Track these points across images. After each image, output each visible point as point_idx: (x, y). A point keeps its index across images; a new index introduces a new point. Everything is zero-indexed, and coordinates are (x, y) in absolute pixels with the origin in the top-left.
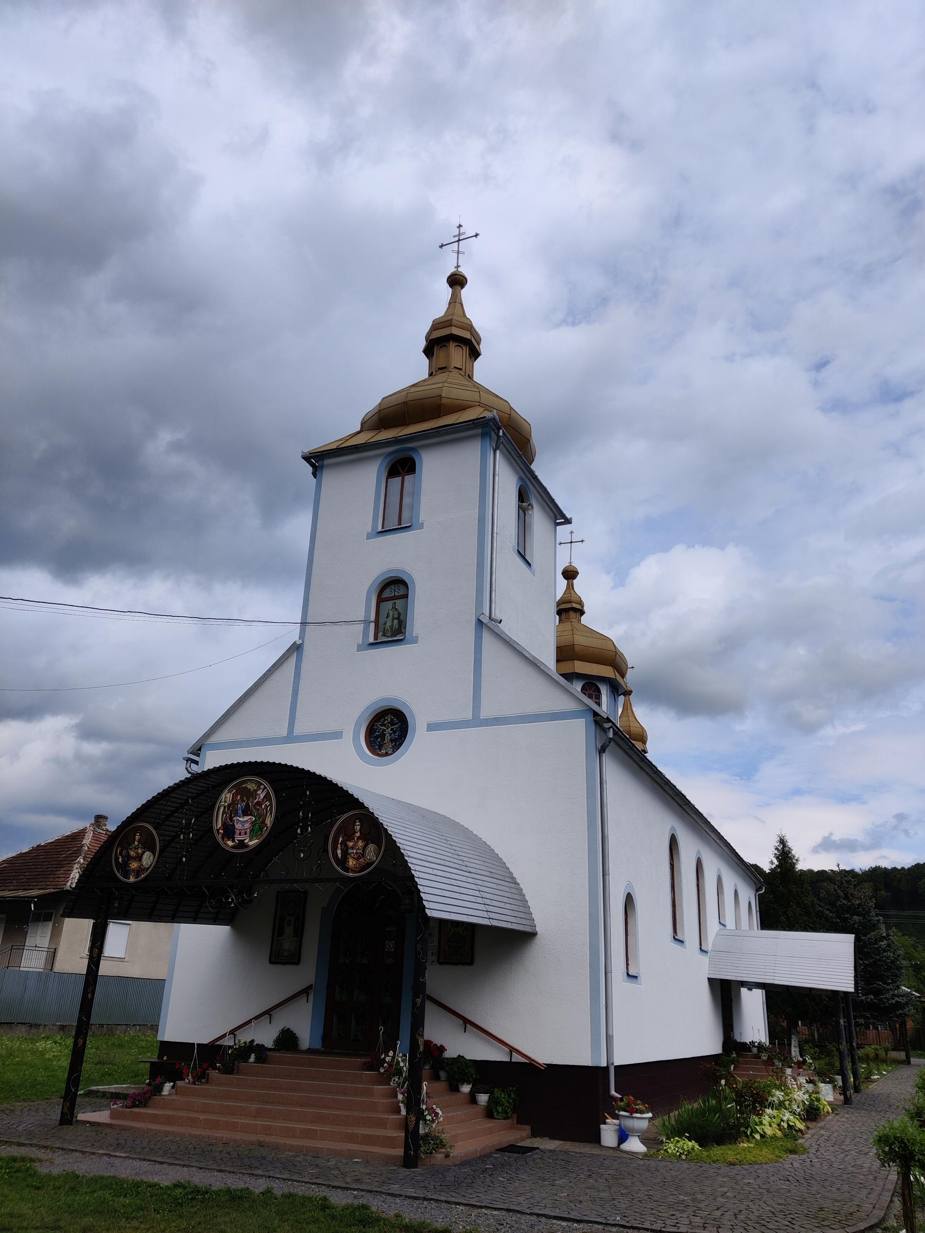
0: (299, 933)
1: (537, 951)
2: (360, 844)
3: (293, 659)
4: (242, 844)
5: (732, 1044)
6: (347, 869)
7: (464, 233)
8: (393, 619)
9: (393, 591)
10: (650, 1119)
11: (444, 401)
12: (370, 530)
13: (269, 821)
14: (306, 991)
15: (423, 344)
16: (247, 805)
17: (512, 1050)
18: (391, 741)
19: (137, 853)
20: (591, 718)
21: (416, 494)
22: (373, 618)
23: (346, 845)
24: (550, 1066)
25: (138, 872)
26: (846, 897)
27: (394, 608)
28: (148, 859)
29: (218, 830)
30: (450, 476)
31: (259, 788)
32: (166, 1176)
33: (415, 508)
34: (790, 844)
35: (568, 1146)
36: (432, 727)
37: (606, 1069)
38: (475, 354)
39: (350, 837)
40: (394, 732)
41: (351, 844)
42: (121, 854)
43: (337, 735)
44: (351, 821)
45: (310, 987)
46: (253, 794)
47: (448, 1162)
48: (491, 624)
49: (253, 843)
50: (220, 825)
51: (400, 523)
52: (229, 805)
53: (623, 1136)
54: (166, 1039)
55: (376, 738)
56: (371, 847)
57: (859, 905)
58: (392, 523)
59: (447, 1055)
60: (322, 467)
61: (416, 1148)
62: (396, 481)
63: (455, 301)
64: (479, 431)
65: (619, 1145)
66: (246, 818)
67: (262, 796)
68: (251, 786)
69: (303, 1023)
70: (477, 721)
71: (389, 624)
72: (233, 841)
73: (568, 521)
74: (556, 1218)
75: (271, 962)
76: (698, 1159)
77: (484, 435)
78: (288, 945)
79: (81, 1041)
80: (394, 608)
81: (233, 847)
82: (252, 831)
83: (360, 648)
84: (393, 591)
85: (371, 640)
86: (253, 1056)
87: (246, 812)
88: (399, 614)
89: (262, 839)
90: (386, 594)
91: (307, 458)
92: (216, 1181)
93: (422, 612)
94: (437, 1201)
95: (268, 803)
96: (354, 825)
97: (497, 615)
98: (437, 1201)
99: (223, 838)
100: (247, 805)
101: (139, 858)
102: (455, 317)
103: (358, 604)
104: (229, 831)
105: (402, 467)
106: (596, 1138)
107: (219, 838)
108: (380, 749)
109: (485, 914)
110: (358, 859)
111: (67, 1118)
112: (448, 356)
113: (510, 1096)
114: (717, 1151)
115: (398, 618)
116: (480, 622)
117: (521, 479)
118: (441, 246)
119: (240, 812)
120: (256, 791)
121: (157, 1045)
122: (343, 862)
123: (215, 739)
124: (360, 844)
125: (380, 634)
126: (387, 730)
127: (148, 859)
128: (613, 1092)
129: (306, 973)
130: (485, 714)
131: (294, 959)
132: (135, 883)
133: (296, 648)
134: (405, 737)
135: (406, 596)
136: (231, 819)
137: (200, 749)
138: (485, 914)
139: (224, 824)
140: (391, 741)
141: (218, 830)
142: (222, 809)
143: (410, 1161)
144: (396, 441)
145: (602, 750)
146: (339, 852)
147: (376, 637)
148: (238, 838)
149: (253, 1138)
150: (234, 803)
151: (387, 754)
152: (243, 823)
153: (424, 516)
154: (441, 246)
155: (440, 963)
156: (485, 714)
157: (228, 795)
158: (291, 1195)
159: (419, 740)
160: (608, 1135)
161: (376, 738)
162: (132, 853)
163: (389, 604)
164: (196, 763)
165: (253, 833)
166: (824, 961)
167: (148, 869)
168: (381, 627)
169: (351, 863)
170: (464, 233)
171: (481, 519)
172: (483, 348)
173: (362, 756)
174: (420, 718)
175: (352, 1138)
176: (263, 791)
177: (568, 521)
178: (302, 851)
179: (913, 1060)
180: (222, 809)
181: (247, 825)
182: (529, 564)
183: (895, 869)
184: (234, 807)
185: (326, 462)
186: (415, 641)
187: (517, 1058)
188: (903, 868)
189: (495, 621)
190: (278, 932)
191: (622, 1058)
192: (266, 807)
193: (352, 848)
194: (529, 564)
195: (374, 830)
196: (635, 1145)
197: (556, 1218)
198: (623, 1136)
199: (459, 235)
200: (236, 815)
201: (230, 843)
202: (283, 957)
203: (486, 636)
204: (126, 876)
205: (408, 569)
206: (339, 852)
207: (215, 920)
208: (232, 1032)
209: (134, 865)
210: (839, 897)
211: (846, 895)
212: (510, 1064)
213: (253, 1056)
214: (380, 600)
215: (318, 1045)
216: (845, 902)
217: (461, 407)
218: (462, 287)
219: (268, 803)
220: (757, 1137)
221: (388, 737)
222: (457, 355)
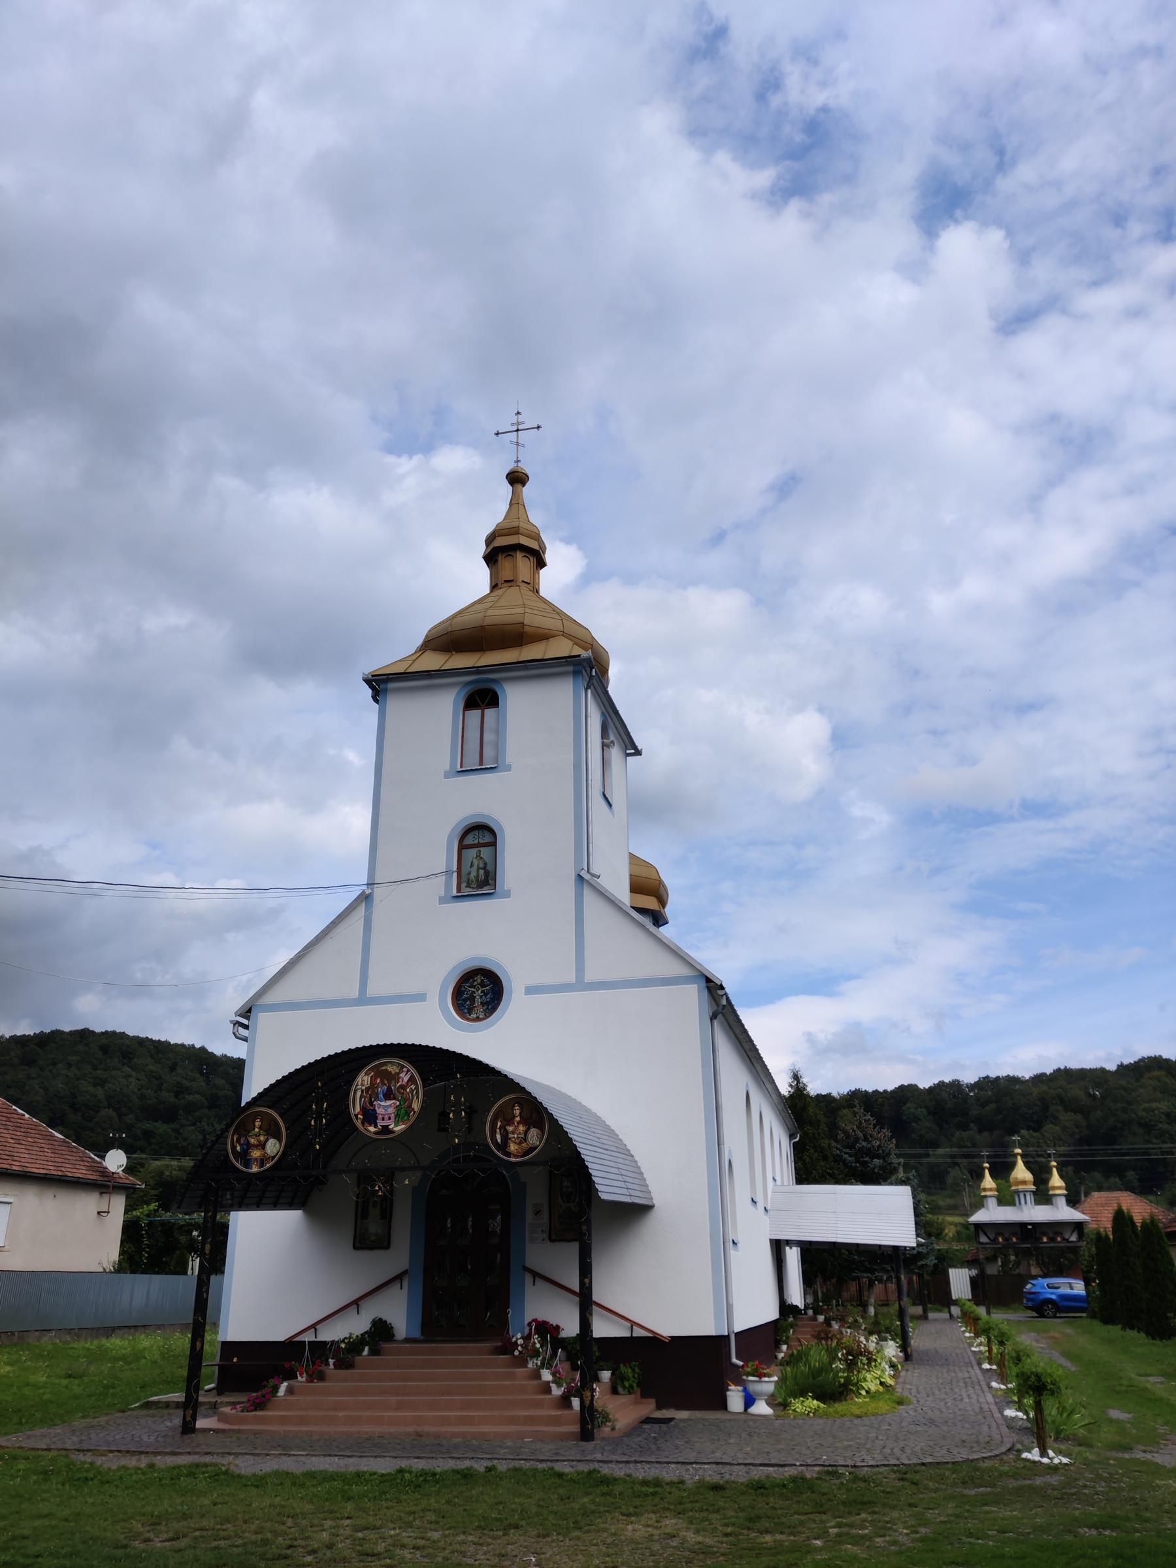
0: (387, 1214)
1: (651, 1226)
2: (521, 1128)
3: (361, 911)
4: (386, 1130)
5: (786, 1308)
6: (508, 1154)
7: (523, 423)
8: (479, 868)
9: (478, 838)
10: (776, 1382)
11: (527, 629)
12: (448, 768)
13: (416, 1106)
14: (399, 1278)
15: (482, 548)
16: (389, 1089)
17: (633, 1324)
18: (483, 1004)
19: (259, 1141)
20: (704, 984)
21: (500, 731)
22: (455, 868)
23: (506, 1130)
24: (672, 1337)
25: (262, 1162)
26: (866, 1139)
27: (479, 856)
28: (273, 1147)
29: (356, 1116)
30: (536, 713)
31: (401, 1071)
32: (384, 1466)
33: (499, 746)
34: (805, 1080)
35: (698, 1414)
36: (530, 990)
37: (728, 1336)
38: (541, 564)
39: (510, 1121)
40: (486, 995)
41: (510, 1129)
42: (238, 1141)
43: (420, 997)
44: (511, 1104)
45: (405, 1273)
46: (396, 1077)
47: (615, 1434)
48: (593, 881)
49: (400, 1128)
50: (358, 1109)
51: (481, 763)
52: (368, 1089)
53: (749, 1401)
54: (229, 1340)
55: (465, 1000)
56: (533, 1132)
57: (879, 1146)
58: (472, 762)
59: (563, 1335)
60: (386, 691)
61: (590, 1423)
62: (474, 715)
63: (516, 503)
64: (571, 668)
65: (746, 1409)
66: (389, 1103)
67: (406, 1079)
68: (392, 1069)
69: (398, 1311)
70: (580, 985)
71: (473, 874)
72: (376, 1126)
73: (638, 753)
74: (761, 1465)
75: (355, 1248)
76: (826, 1415)
77: (576, 673)
78: (374, 1228)
79: (198, 1344)
80: (479, 856)
81: (375, 1133)
82: (397, 1116)
83: (442, 900)
84: (478, 838)
85: (454, 892)
86: (367, 1348)
87: (388, 1095)
88: (486, 864)
89: (409, 1123)
90: (469, 840)
91: (368, 681)
92: (443, 1465)
93: (513, 863)
94: (648, 1462)
95: (413, 1087)
96: (513, 1109)
97: (594, 870)
98: (648, 1462)
99: (363, 1124)
100: (389, 1089)
101: (263, 1146)
102: (522, 525)
103: (439, 855)
104: (370, 1116)
105: (482, 698)
106: (723, 1405)
107: (359, 1124)
108: (470, 1012)
109: (625, 1191)
110: (520, 1144)
111: (188, 1428)
112: (515, 567)
113: (633, 1371)
114: (839, 1407)
115: (484, 868)
116: (580, 878)
117: (603, 713)
118: (497, 434)
119: (381, 1096)
120: (398, 1074)
121: (219, 1347)
122: (503, 1147)
123: (269, 999)
124: (521, 1128)
125: (464, 885)
126: (479, 991)
127: (273, 1147)
128: (734, 1360)
129: (398, 1257)
130: (589, 977)
131: (382, 1243)
132: (258, 1173)
133: (365, 898)
134: (499, 1004)
135: (494, 844)
136: (371, 1103)
137: (249, 1011)
138: (625, 1191)
139: (364, 1110)
140: (483, 1004)
141: (356, 1116)
142: (359, 1093)
143: (586, 1435)
144: (477, 670)
145: (714, 1017)
146: (498, 1137)
147: (459, 890)
148: (380, 1123)
149: (411, 1429)
150: (372, 1087)
151: (478, 1019)
152: (385, 1108)
153: (510, 757)
154: (497, 434)
155: (551, 1240)
156: (589, 977)
157: (366, 1078)
158: (516, 1469)
159: (515, 1003)
160: (735, 1399)
161: (465, 1000)
162: (252, 1141)
163: (473, 852)
164: (246, 1027)
165: (398, 1118)
166: (879, 1215)
167: (273, 1157)
168: (464, 878)
169: (513, 1147)
170: (523, 423)
171: (577, 766)
172: (548, 557)
173: (451, 1022)
174: (515, 981)
175: (512, 1421)
176: (406, 1074)
177: (638, 753)
178: (456, 1136)
179: (931, 1315)
180: (359, 1093)
181: (391, 1110)
182: (610, 805)
183: (876, 1091)
184: (373, 1091)
185: (391, 685)
186: (507, 895)
187: (639, 1332)
188: (885, 1091)
189: (593, 875)
190: (362, 1213)
191: (740, 1325)
192: (412, 1091)
193: (513, 1133)
194: (610, 805)
195: (534, 1111)
196: (762, 1408)
197: (761, 1465)
198: (749, 1401)
199: (518, 423)
200: (377, 1099)
201: (372, 1129)
202: (368, 1240)
203: (588, 893)
204: (247, 1164)
205: (485, 812)
206: (498, 1137)
207: (290, 1206)
208: (314, 1326)
209: (256, 1154)
210: (857, 1139)
211: (865, 1136)
212: (631, 1340)
213: (367, 1348)
214: (462, 847)
215: (417, 1334)
216: (864, 1144)
217: (543, 636)
218: (524, 484)
219: (413, 1087)
220: (863, 1393)
221: (478, 1001)
222: (523, 564)
